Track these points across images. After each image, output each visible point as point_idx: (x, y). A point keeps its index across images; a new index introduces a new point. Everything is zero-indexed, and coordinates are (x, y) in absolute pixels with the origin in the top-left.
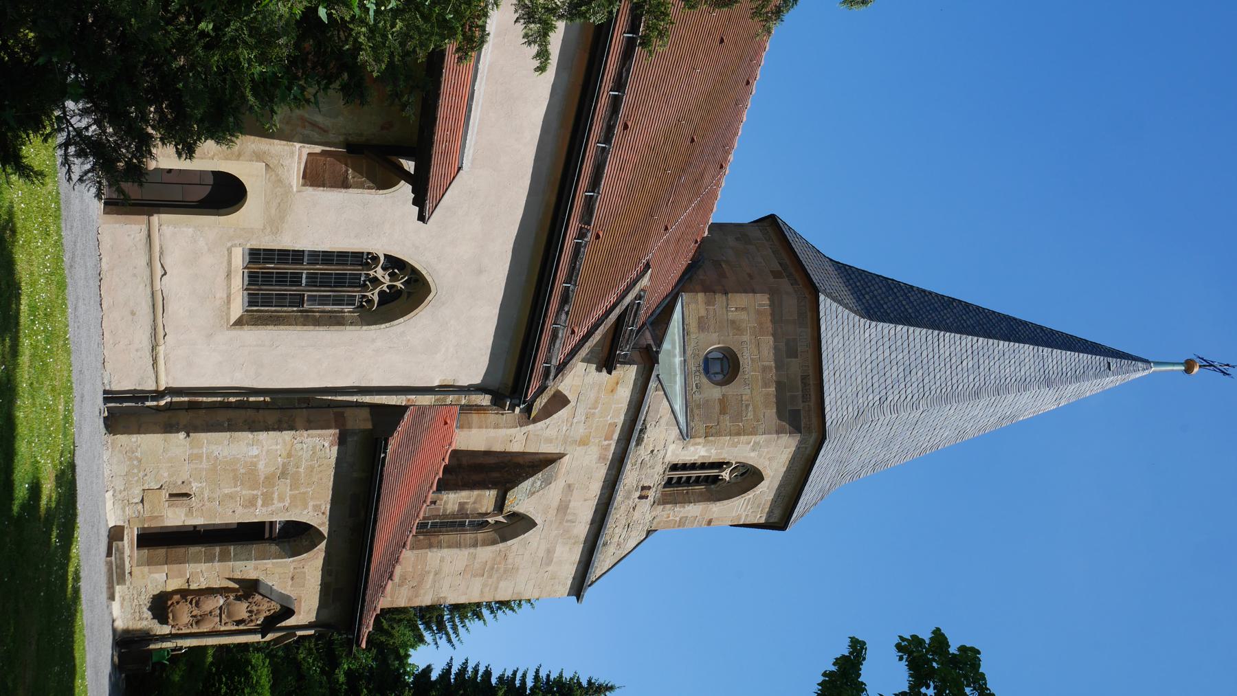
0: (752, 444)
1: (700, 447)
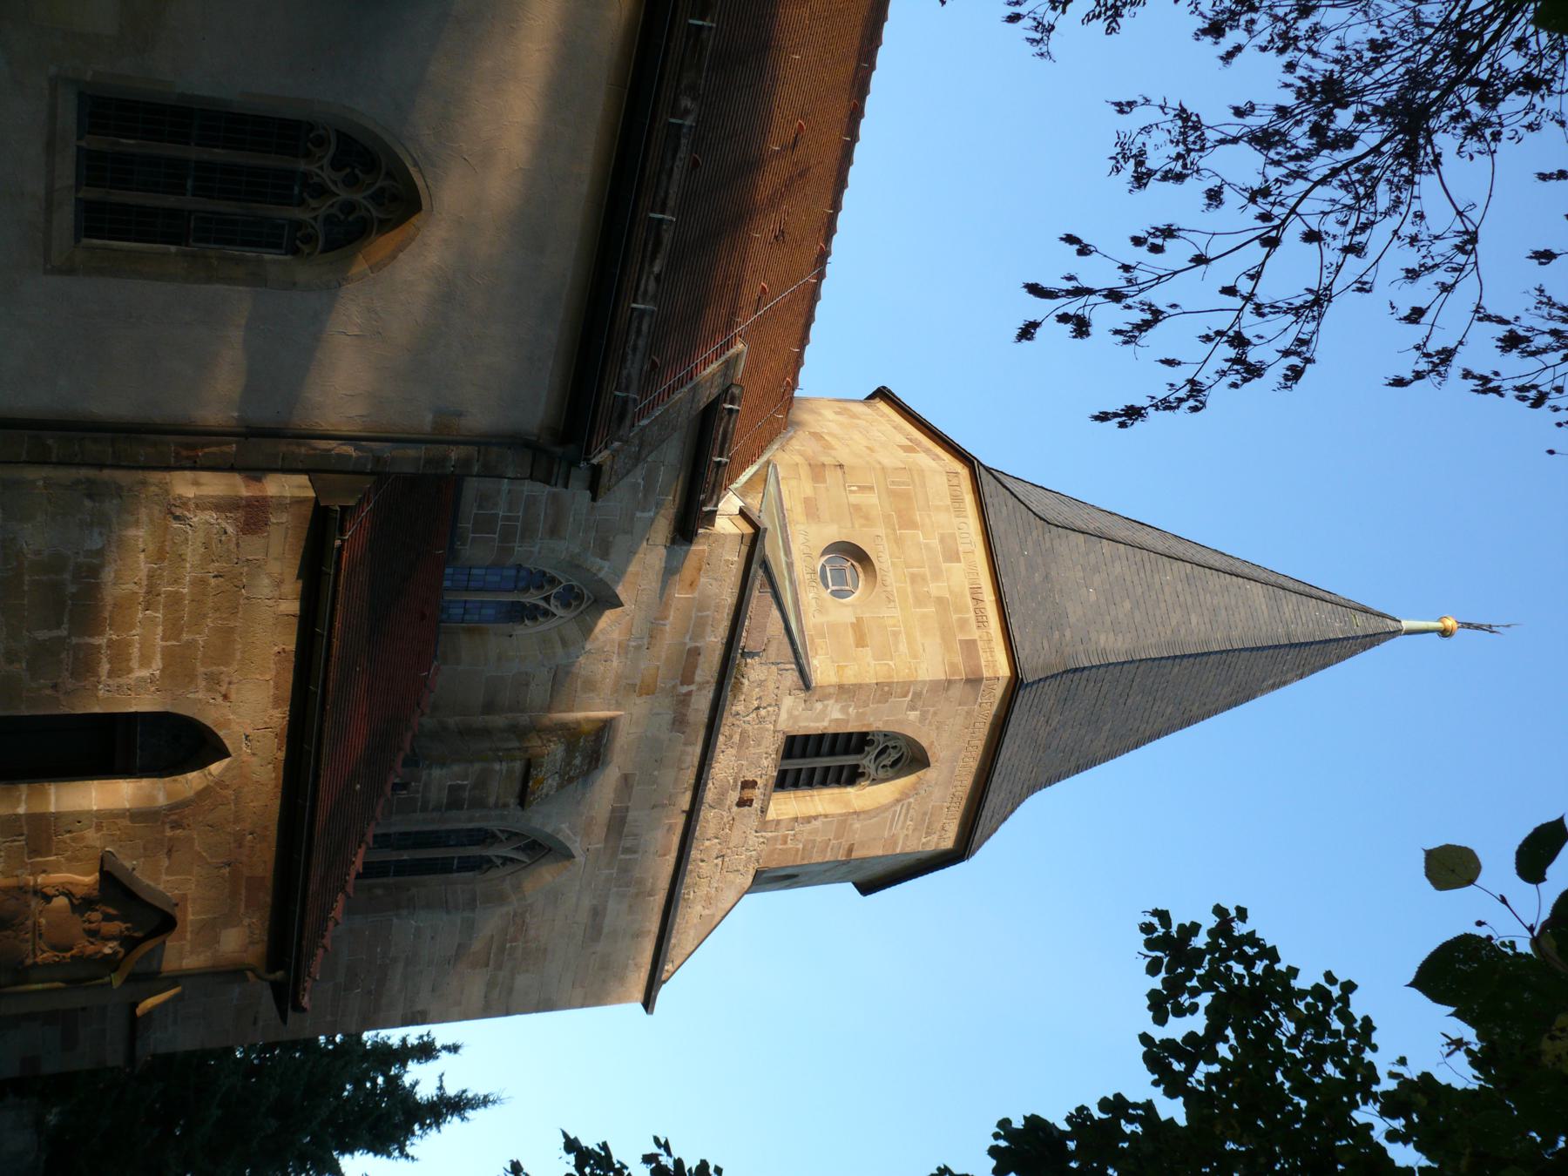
0: (910, 694)
1: (831, 702)
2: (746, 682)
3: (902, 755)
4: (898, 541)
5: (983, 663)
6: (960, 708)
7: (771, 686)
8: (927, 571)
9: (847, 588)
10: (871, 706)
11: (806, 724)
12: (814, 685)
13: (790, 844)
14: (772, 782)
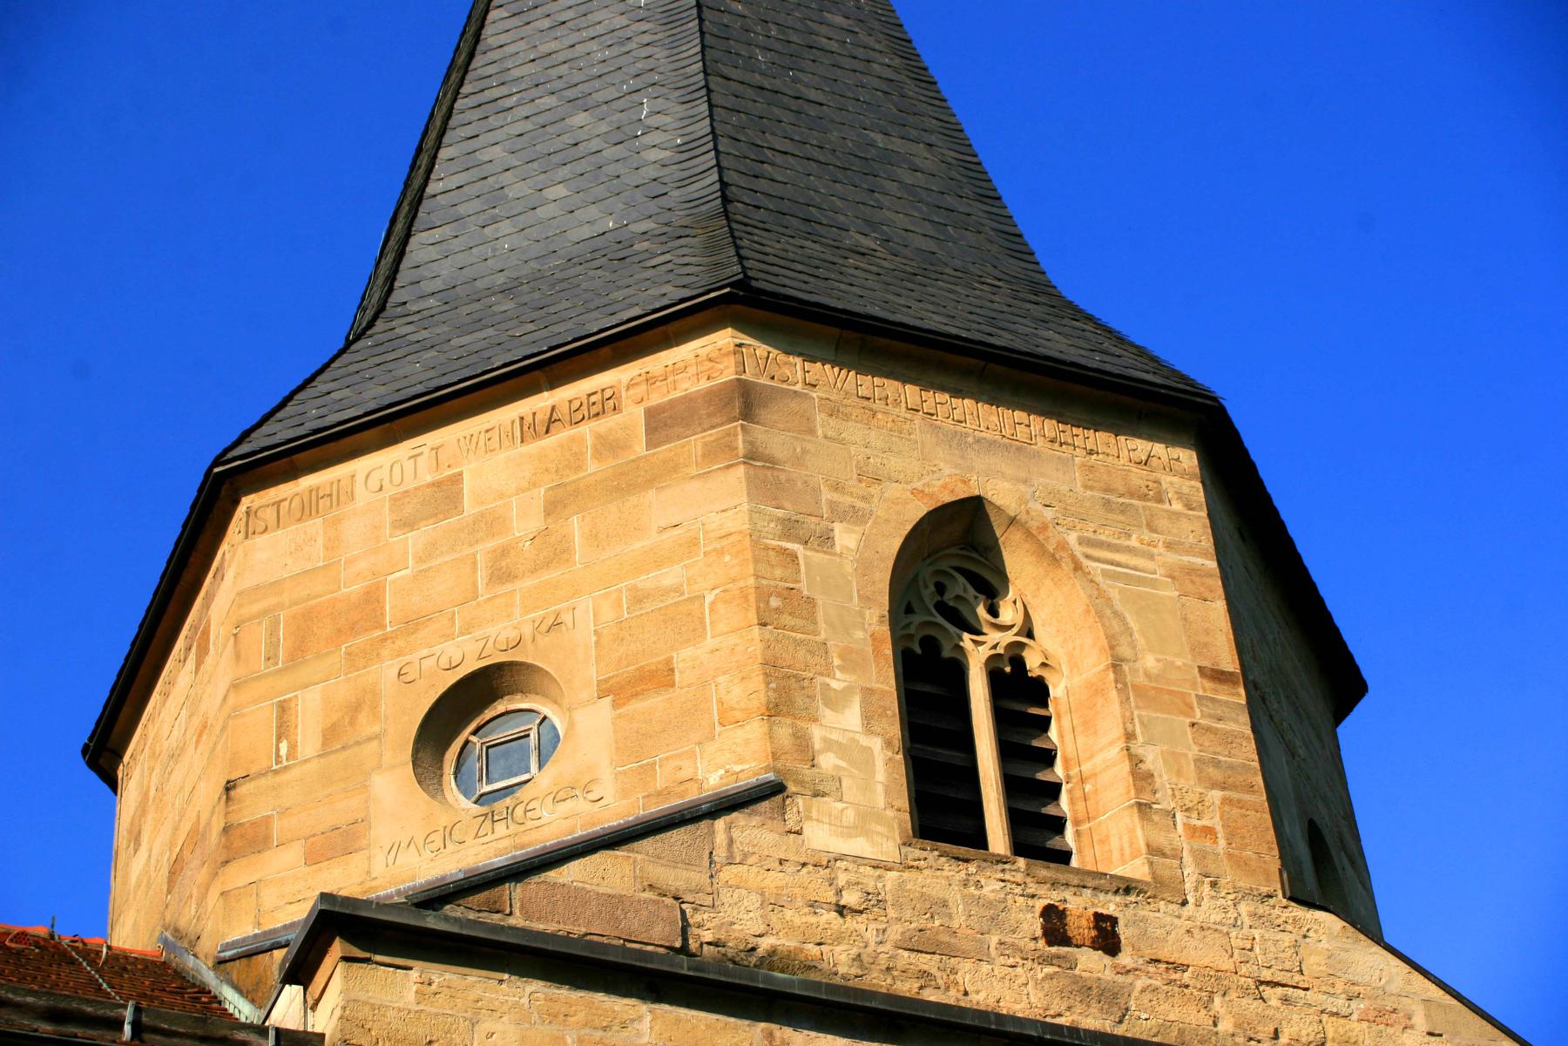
0: (789, 545)
1: (817, 734)
2: (765, 944)
3: (958, 569)
4: (412, 624)
5: (704, 384)
6: (820, 432)
7: (774, 880)
8: (483, 549)
9: (533, 735)
10: (823, 636)
11: (880, 789)
12: (771, 776)
13: (1213, 820)
14: (1044, 871)
